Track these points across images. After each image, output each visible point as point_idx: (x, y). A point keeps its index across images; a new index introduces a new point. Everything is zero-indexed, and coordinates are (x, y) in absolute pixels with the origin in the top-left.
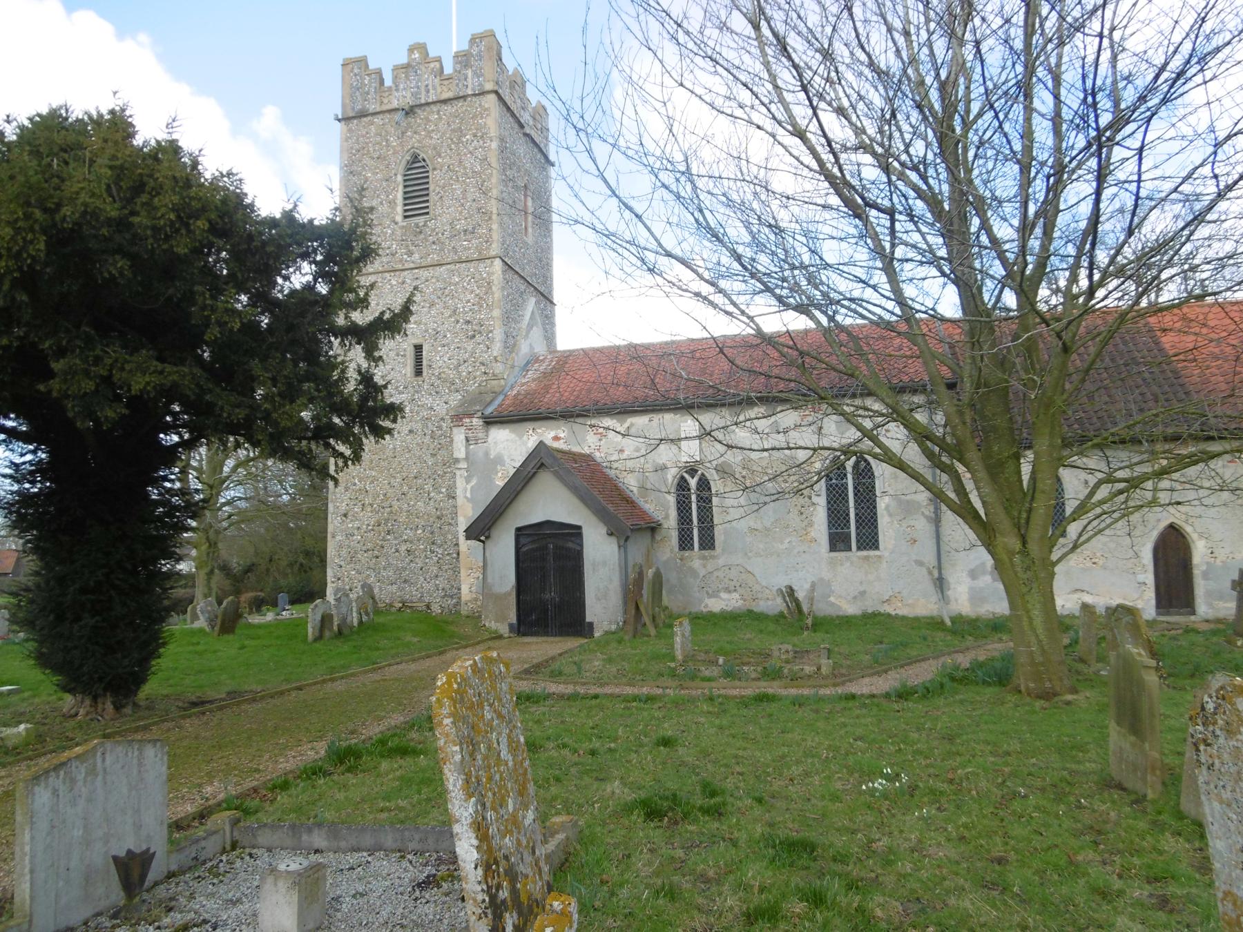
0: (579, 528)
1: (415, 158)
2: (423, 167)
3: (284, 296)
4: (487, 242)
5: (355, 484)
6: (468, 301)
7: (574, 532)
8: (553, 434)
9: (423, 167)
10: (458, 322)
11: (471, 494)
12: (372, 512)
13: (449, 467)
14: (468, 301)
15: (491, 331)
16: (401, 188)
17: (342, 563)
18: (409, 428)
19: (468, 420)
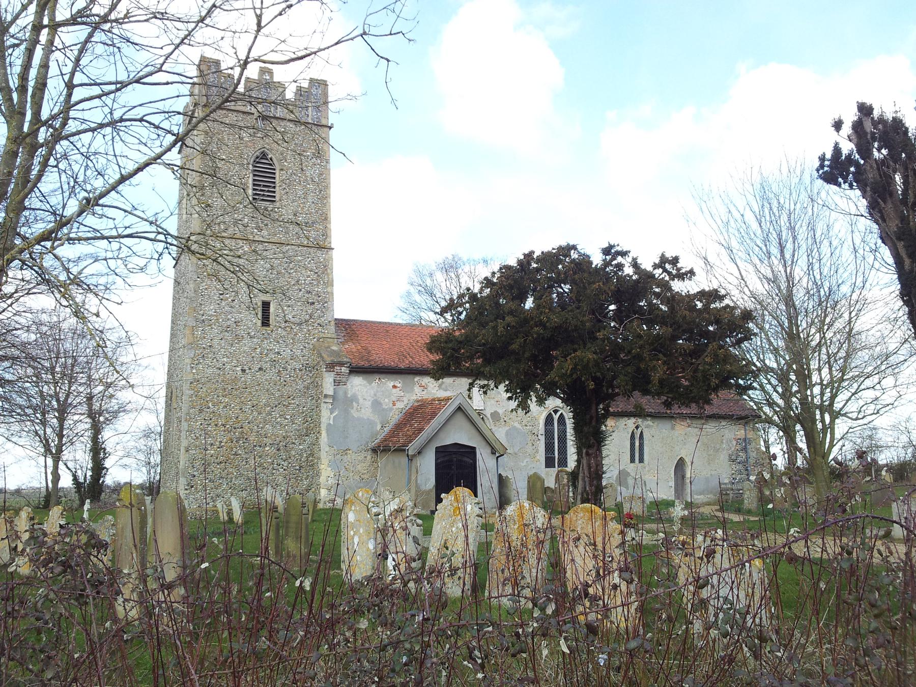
0: (474, 448)
1: (264, 155)
2: (270, 165)
3: (481, 296)
4: (323, 235)
5: (209, 408)
6: (308, 277)
7: (471, 451)
8: (392, 384)
9: (270, 165)
10: (301, 290)
11: (333, 422)
12: (225, 431)
13: (293, 399)
14: (308, 277)
15: (326, 302)
16: (277, 180)
17: (195, 473)
18: (259, 366)
19: (339, 368)
